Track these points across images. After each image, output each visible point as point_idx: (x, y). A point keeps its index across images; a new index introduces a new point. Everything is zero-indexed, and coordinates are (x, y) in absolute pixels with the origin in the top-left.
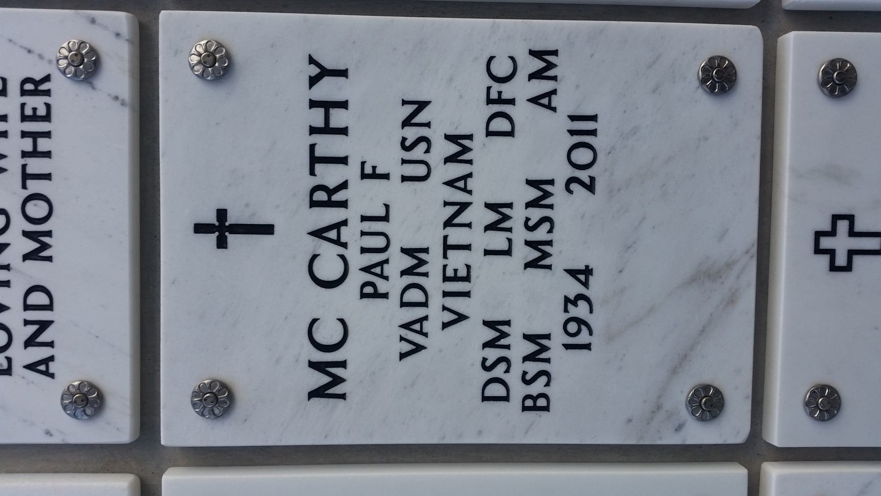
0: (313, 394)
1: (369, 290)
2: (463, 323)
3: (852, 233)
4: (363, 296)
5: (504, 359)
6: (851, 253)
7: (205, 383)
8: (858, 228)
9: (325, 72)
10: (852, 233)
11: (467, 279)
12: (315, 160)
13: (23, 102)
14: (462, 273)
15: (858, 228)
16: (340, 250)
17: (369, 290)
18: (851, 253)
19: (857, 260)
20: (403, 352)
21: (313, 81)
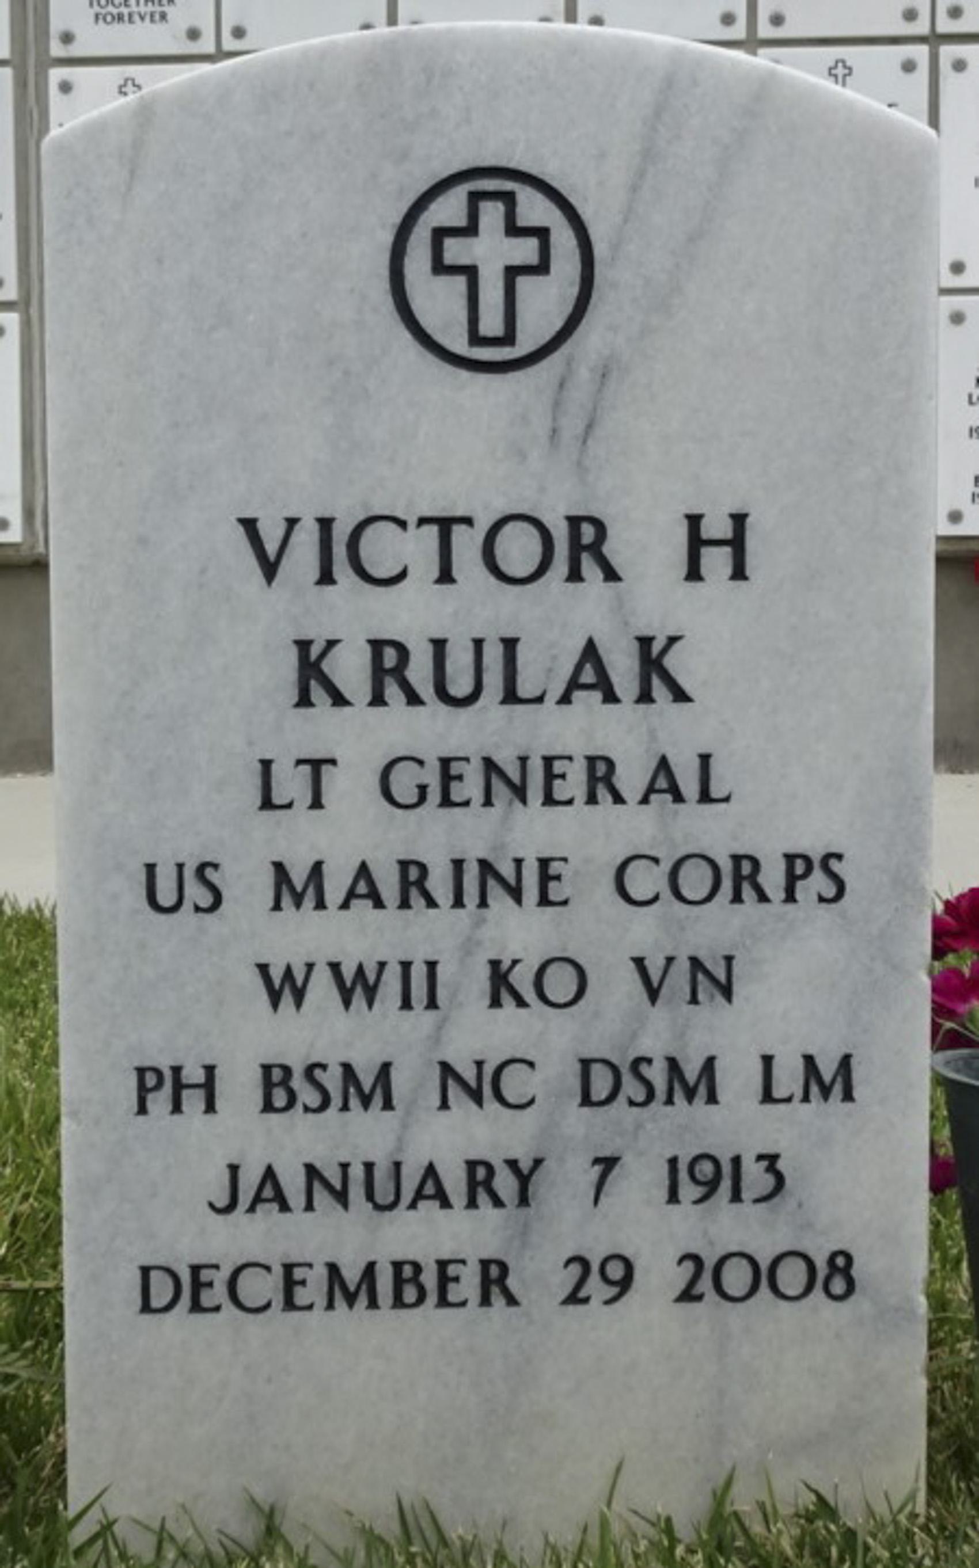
0: (279, 868)
1: (151, 1080)
2: (645, 996)
3: (512, 273)
4: (141, 1071)
5: (651, 1095)
6: (471, 272)
7: (47, 1039)
8: (523, 283)
9: (524, 1180)
10: (512, 273)
11: (544, 900)
12: (445, 525)
13: (469, 1263)
14: (555, 891)
15: (523, 283)
16: (557, 689)
17: (151, 1080)
18: (471, 272)
19: (460, 282)
20: (647, 962)
21: (512, 1164)
